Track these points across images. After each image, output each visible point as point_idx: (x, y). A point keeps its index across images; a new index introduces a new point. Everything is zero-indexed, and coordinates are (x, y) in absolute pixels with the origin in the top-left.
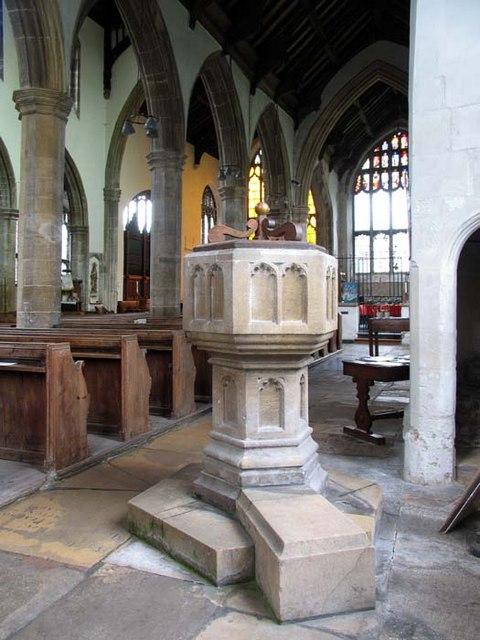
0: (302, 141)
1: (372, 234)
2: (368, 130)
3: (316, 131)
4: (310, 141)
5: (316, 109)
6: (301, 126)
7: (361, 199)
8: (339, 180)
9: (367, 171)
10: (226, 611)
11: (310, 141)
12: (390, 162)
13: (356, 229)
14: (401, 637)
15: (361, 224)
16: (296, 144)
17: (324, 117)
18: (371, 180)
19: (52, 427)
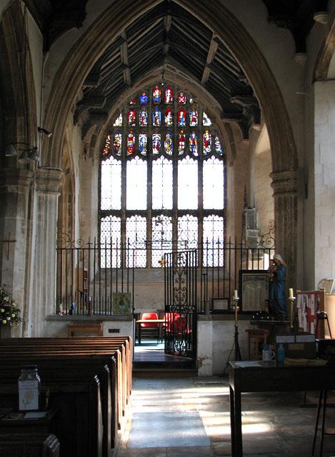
0: (55, 69)
1: (124, 214)
2: (127, 74)
3: (75, 58)
4: (67, 72)
5: (79, 25)
6: (52, 47)
7: (110, 168)
8: (83, 138)
9: (120, 130)
10: (134, 453)
11: (67, 72)
12: (150, 119)
13: (103, 208)
14: (314, 74)
15: (110, 200)
16: (45, 71)
17: (90, 38)
18: (124, 142)
19: (53, 259)
